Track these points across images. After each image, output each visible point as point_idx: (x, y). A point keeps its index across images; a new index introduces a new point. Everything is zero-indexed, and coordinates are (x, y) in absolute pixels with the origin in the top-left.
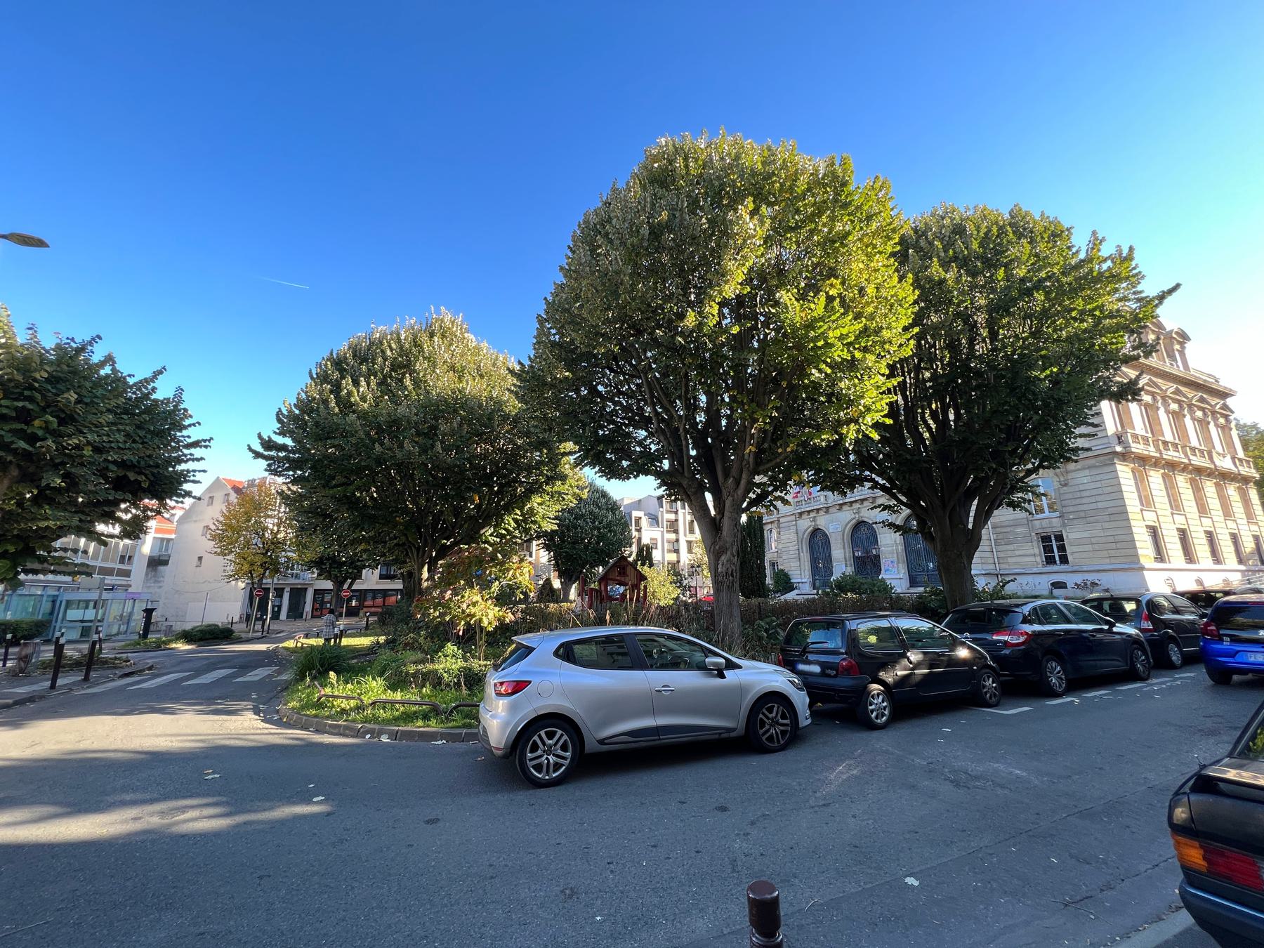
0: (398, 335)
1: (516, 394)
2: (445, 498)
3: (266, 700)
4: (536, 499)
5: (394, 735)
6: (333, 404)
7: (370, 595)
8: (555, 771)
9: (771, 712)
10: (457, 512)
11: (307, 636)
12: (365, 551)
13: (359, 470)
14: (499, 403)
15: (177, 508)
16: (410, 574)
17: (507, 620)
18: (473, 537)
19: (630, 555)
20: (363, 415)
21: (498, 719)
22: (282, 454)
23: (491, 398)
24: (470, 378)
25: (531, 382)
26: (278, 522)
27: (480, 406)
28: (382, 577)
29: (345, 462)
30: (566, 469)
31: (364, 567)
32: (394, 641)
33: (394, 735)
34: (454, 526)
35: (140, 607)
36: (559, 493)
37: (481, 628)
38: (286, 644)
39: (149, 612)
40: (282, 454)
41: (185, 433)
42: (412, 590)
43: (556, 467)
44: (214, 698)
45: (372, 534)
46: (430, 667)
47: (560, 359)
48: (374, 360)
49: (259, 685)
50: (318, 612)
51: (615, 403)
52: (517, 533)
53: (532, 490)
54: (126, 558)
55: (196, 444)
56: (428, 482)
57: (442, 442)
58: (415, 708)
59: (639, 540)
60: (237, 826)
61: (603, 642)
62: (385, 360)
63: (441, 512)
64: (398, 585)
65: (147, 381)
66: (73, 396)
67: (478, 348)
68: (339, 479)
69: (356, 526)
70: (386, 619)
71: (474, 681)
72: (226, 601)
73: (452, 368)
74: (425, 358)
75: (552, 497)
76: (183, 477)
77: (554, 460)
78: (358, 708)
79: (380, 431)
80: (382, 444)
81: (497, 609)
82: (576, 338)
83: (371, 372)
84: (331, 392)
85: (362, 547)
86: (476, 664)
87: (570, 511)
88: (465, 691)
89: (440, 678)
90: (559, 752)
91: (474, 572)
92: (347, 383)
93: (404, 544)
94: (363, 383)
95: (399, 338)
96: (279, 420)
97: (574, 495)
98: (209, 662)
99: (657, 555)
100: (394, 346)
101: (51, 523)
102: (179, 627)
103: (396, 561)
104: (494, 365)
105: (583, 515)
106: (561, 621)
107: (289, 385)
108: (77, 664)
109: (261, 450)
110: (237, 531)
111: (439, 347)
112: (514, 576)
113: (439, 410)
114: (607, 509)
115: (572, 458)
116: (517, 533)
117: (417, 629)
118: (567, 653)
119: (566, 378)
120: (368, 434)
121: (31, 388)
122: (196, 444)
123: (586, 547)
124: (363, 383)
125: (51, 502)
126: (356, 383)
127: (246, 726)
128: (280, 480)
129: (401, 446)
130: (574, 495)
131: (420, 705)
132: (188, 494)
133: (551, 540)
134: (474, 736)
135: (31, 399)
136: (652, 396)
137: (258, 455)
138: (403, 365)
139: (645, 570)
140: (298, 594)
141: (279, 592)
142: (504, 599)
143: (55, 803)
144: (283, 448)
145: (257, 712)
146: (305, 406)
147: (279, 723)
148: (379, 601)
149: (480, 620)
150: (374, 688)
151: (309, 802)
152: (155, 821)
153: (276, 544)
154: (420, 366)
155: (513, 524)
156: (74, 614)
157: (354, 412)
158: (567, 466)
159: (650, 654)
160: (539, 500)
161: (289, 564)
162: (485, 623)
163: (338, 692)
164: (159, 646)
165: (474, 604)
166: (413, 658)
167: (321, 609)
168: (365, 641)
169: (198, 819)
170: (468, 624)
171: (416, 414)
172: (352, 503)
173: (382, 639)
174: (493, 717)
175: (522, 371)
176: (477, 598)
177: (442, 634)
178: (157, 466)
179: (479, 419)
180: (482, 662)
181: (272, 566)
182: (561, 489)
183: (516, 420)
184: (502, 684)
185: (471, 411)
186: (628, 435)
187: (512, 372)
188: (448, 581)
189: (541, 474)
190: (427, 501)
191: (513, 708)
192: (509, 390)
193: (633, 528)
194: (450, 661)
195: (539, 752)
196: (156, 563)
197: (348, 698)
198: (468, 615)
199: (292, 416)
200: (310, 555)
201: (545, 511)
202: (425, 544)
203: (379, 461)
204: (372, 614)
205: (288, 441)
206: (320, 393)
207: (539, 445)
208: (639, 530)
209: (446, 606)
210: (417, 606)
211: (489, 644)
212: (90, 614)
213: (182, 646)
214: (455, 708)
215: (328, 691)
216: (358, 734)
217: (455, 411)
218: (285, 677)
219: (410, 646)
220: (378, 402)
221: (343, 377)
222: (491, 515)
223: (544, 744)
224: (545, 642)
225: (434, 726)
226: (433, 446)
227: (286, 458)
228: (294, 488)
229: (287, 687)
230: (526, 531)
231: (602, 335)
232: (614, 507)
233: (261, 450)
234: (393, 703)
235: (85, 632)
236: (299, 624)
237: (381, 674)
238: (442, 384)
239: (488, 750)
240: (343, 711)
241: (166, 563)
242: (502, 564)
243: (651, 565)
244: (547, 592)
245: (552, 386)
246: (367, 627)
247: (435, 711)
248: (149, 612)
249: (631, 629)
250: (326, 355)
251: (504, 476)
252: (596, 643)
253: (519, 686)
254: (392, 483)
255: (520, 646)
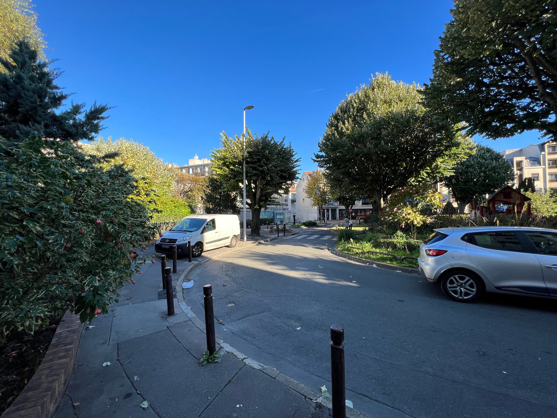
0: (358, 95)
1: (423, 104)
2: (389, 166)
3: (331, 246)
4: (439, 160)
5: (378, 265)
6: (336, 135)
7: (359, 211)
8: (465, 296)
9: (470, 286)
10: (395, 172)
11: (339, 226)
12: (355, 193)
13: (350, 160)
14: (413, 112)
15: (296, 183)
16: (375, 202)
17: (428, 222)
18: (404, 183)
19: (513, 185)
20: (349, 136)
21: (429, 266)
22: (322, 159)
23: (408, 111)
24: (395, 104)
25: (432, 94)
26: (324, 185)
27: (402, 117)
28: (363, 204)
29: (344, 158)
30: (460, 139)
31: (356, 200)
32: (372, 229)
33: (378, 265)
34: (393, 179)
35: (292, 215)
36: (455, 154)
37: (414, 226)
38: (333, 228)
39: (294, 216)
40: (322, 159)
41: (294, 157)
42: (377, 207)
43: (452, 139)
44: (317, 243)
45: (358, 186)
46: (390, 240)
47: (453, 72)
48: (349, 110)
49: (328, 241)
50: (341, 218)
51: (499, 87)
52: (428, 179)
53: (439, 154)
54: (286, 200)
55: (297, 161)
56: (379, 161)
57: (384, 140)
58: (385, 256)
59: (521, 176)
60: (331, 283)
61: (496, 235)
62: (354, 109)
63: (386, 173)
64: (370, 207)
65: (282, 142)
66: (267, 152)
67: (398, 87)
68: (343, 165)
69: (351, 184)
70: (366, 221)
71: (413, 249)
72: (313, 214)
73: (385, 102)
74: (371, 102)
75: (450, 157)
76: (295, 173)
77: (450, 136)
78: (363, 253)
79: (355, 141)
80: (357, 147)
81: (421, 216)
82: (466, 53)
83: (349, 116)
84: (335, 130)
85: (354, 192)
86: (413, 241)
87: (462, 164)
88: (408, 252)
89: (395, 245)
90: (468, 287)
91: (408, 199)
92: (340, 124)
93: (371, 189)
94: (346, 122)
95: (359, 97)
96: (320, 147)
97: (466, 154)
98: (310, 232)
99: (538, 185)
100: (357, 101)
101: (270, 191)
102: (302, 222)
103: (368, 197)
104: (408, 92)
105: (472, 165)
106: (461, 223)
107: (321, 132)
108: (282, 231)
109: (315, 159)
110: (312, 189)
111: (378, 93)
112: (431, 201)
113: (380, 125)
114: (492, 159)
115: (463, 132)
116: (428, 179)
117: (382, 224)
118: (470, 239)
119: (458, 83)
120: (351, 144)
121: (259, 152)
122: (297, 161)
123: (475, 184)
124: (346, 122)
125: (269, 185)
126: (344, 123)
127: (326, 254)
128: (323, 169)
129: (365, 146)
130: (466, 154)
131: (388, 255)
132: (298, 178)
133: (449, 182)
134: (417, 272)
135: (259, 155)
136: (537, 69)
137: (315, 161)
138: (362, 109)
139: (529, 194)
140: (334, 210)
141: (328, 210)
142: (427, 211)
143: (285, 266)
144: (322, 156)
145: (329, 250)
146: (327, 138)
147: (336, 254)
148: (363, 214)
149: (413, 221)
150: (367, 246)
151: (351, 282)
152: (309, 276)
153: (324, 193)
154: (370, 106)
155: (425, 175)
156: (278, 217)
157: (345, 136)
158: (459, 138)
159: (538, 245)
160: (441, 160)
161: (329, 200)
162: (415, 223)
163: (355, 246)
164: (298, 227)
165: (409, 214)
166: (382, 236)
167: (342, 216)
168: (361, 229)
169: (319, 279)
170: (406, 223)
171: (370, 130)
172: (348, 174)
173: (367, 228)
174: (427, 264)
175: (427, 89)
176: (410, 211)
177: (394, 227)
178: (289, 170)
179: (403, 123)
180: (415, 240)
181: (324, 201)
182: (456, 151)
183: (424, 119)
184: (430, 250)
185: (397, 121)
186: (513, 106)
187: (420, 92)
188: (393, 204)
189: (442, 145)
190: (379, 169)
191: (437, 262)
192: (418, 103)
193: (515, 168)
194: (400, 239)
195: (455, 285)
196: (293, 201)
197: (358, 249)
198: (407, 219)
199: (324, 144)
200: (336, 197)
201: (446, 166)
202: (381, 189)
203: (357, 155)
204: (361, 219)
205: (323, 154)
206: (331, 132)
207: (439, 130)
208: (521, 169)
209: (395, 215)
210: (381, 215)
211: (418, 233)
212: (282, 217)
213: (304, 227)
214: (404, 258)
215: (350, 245)
216: (363, 262)
217: (389, 123)
218: (335, 239)
219: (380, 231)
220: (353, 128)
221: (338, 122)
222: (414, 171)
223: (458, 282)
224: (455, 234)
225: (395, 264)
226: (380, 143)
227: (324, 160)
228: (327, 171)
229: (336, 243)
230: (434, 178)
231: (486, 43)
232: (498, 157)
233: (315, 159)
234: (376, 253)
235: (282, 222)
236: (336, 222)
237: (369, 241)
238: (380, 111)
239: (425, 278)
240: (357, 253)
241: (295, 201)
242: (423, 194)
243: (533, 191)
244: (449, 208)
245: (447, 91)
246: (360, 224)
247: (394, 259)
248: (294, 216)
249: (516, 228)
250: (331, 115)
251: (419, 151)
252: (490, 235)
253: (439, 253)
254: (363, 164)
255: (438, 234)
